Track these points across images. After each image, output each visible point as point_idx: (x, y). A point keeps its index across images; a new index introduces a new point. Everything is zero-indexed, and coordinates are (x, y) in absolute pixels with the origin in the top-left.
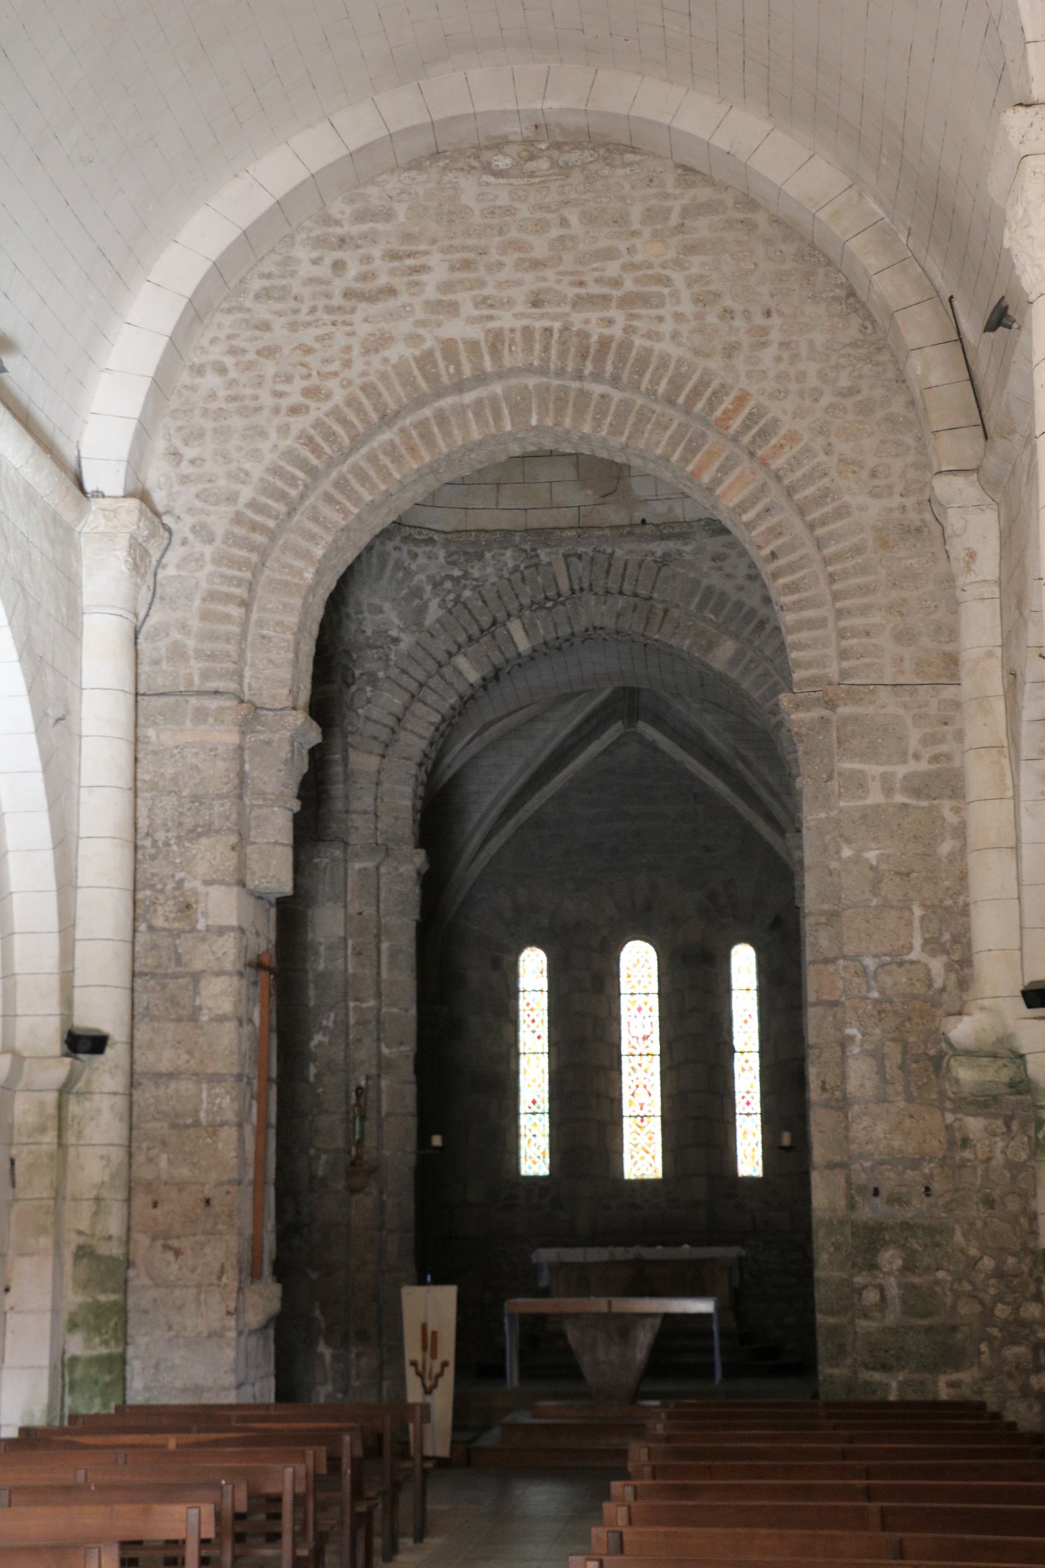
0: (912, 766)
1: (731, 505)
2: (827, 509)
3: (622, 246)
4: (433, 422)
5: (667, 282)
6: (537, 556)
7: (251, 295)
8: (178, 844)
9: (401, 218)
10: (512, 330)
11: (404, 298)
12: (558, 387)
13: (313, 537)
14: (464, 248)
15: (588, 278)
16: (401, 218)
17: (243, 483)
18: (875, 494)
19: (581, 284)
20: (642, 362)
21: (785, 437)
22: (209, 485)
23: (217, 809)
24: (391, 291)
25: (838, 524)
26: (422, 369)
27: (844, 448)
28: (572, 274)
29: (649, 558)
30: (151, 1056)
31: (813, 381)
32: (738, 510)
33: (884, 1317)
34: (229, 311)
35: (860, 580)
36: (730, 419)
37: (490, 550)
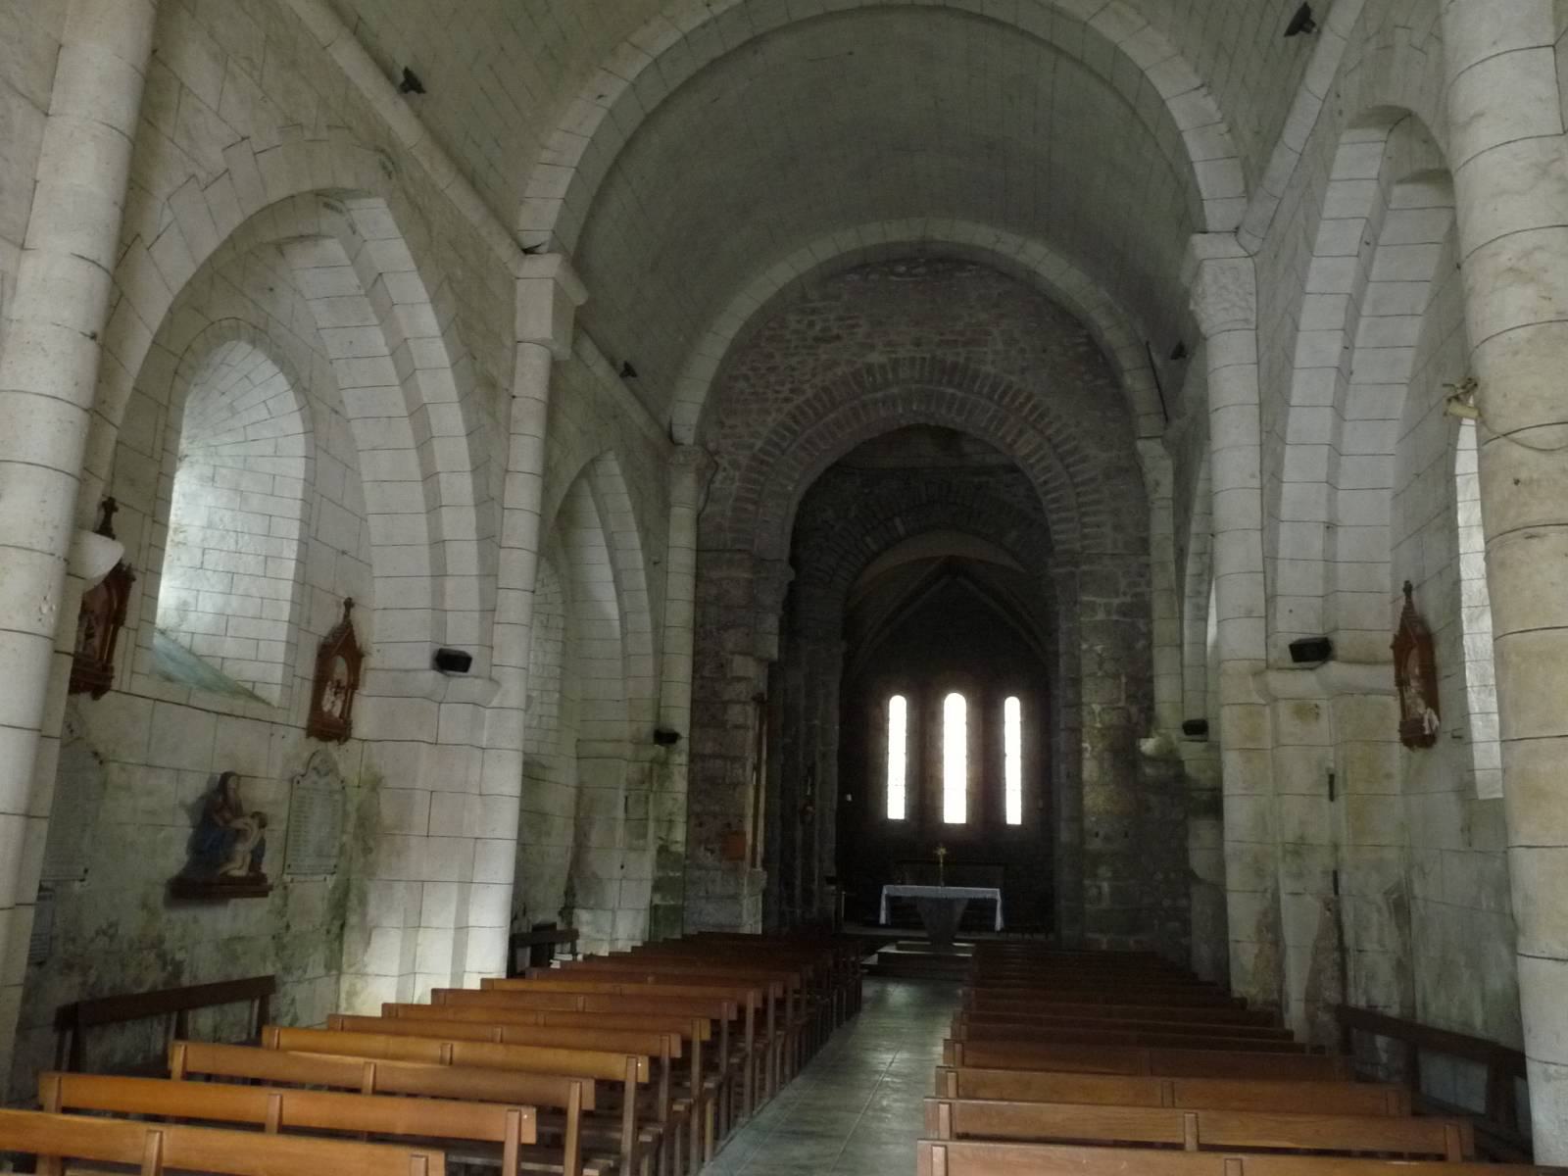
10: (904, 359)
19: (942, 334)
24: (838, 337)
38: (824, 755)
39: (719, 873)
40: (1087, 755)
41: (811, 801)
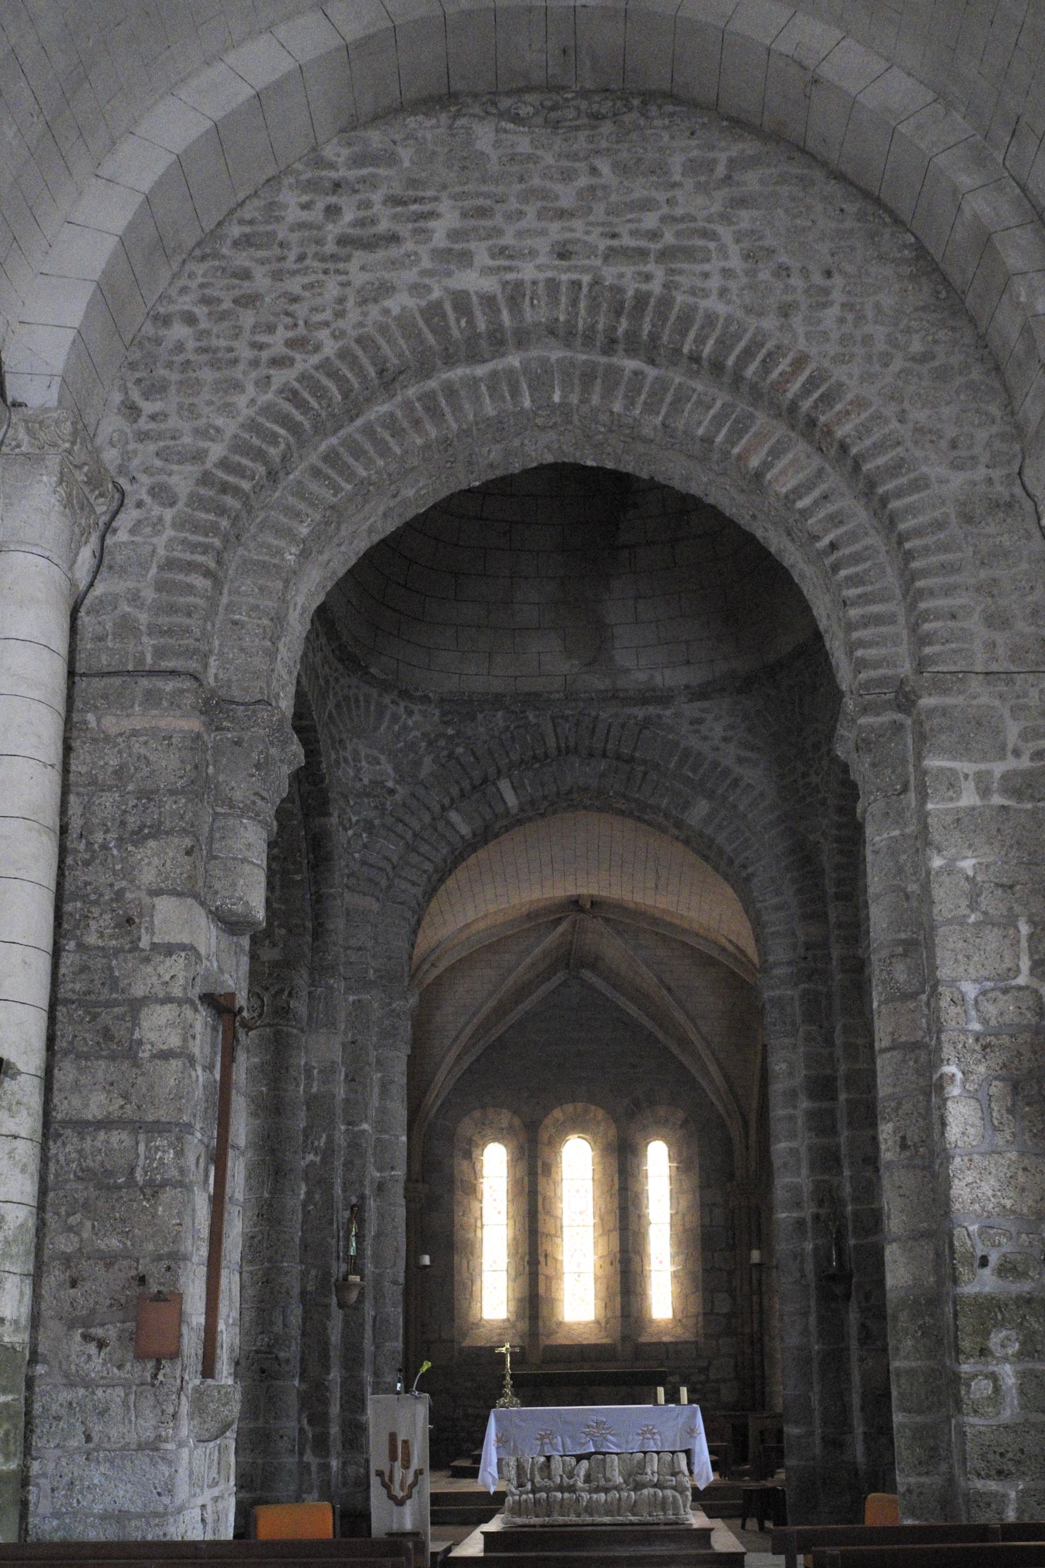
0: (1011, 764)
1: (784, 490)
2: (903, 480)
3: (661, 196)
4: (440, 393)
5: (712, 236)
6: (527, 717)
7: (229, 242)
8: (119, 847)
9: (407, 164)
10: (534, 283)
11: (409, 246)
12: (584, 362)
13: (297, 515)
14: (478, 195)
15: (623, 230)
16: (407, 164)
17: (213, 440)
18: (956, 466)
19: (614, 236)
20: (686, 319)
21: (851, 403)
22: (172, 443)
23: (169, 805)
24: (394, 238)
25: (915, 497)
26: (427, 322)
27: (920, 415)
28: (603, 224)
29: (632, 722)
30: (76, 1101)
31: (880, 346)
32: (792, 496)
33: (999, 1413)
34: (203, 258)
35: (943, 557)
36: (788, 382)
37: (481, 712)
38: (381, 1188)
39: (120, 1391)
40: (954, 1091)
41: (356, 1266)
